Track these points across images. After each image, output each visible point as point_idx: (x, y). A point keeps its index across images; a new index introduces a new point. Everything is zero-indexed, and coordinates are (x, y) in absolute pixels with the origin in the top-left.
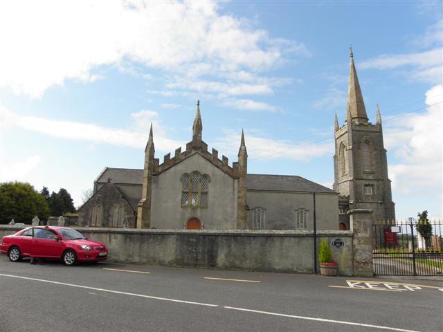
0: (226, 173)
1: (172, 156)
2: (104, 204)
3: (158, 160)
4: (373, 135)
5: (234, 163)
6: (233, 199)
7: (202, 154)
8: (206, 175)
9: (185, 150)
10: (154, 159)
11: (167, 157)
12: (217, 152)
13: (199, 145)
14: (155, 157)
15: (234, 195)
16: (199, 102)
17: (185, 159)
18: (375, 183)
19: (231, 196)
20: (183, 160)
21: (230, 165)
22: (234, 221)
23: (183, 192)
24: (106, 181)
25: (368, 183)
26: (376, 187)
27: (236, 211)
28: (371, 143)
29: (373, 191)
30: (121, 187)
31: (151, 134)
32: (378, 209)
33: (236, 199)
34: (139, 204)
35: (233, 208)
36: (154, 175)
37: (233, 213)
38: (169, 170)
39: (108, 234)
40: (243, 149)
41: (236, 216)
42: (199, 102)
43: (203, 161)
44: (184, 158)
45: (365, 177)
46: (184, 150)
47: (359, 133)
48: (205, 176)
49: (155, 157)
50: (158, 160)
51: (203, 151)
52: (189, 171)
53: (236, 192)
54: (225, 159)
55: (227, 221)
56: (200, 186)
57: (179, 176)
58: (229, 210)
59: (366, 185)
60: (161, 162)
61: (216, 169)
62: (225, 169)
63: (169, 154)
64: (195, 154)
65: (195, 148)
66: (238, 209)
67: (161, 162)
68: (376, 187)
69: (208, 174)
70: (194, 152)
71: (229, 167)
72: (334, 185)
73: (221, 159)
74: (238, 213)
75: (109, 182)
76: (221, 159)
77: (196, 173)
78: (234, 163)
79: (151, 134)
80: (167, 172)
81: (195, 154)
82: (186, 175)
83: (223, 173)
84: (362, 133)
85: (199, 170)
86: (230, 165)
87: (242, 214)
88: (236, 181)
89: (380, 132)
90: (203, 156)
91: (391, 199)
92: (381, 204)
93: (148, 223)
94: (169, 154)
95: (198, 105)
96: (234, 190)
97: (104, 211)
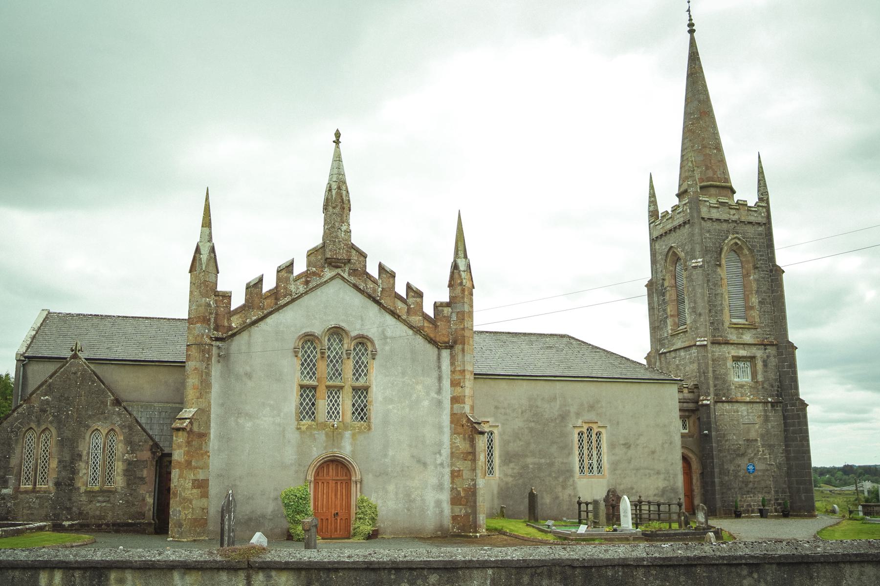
0: (417, 330)
1: (269, 284)
2: (60, 423)
3: (227, 296)
4: (750, 230)
5: (437, 306)
6: (440, 403)
7: (352, 279)
8: (362, 337)
9: (304, 269)
10: (217, 294)
11: (254, 287)
12: (392, 275)
13: (343, 255)
14: (220, 288)
15: (439, 391)
16: (338, 135)
17: (306, 293)
18: (759, 353)
19: (433, 395)
20: (301, 296)
21: (429, 309)
22: (442, 464)
23: (302, 387)
24: (68, 354)
25: (742, 353)
26: (760, 365)
27: (446, 438)
28: (746, 251)
29: (754, 374)
30: (105, 372)
31: (207, 222)
32: (766, 419)
33: (447, 404)
34: (177, 424)
35: (440, 428)
36: (217, 339)
37: (440, 444)
38: (262, 325)
39: (242, 575)
40: (462, 266)
41: (446, 451)
42: (338, 135)
43: (357, 300)
44: (302, 289)
45: (733, 337)
46: (300, 267)
47: (716, 226)
48: (363, 341)
49: (220, 288)
50: (227, 296)
51: (354, 272)
52: (318, 329)
53: (446, 383)
54: (415, 293)
55: (425, 464)
56: (348, 367)
57: (291, 341)
58: (429, 434)
59: (737, 359)
60: (238, 301)
61: (389, 320)
62: (416, 320)
63: (261, 280)
64: (332, 279)
65: (332, 263)
66: (454, 432)
67: (238, 301)
68: (760, 365)
69: (370, 335)
70: (328, 273)
71: (426, 317)
72: (648, 358)
73: (402, 292)
74: (452, 443)
75: (75, 356)
76: (402, 292)
77: (337, 332)
78: (437, 306)
79: (207, 222)
80: (255, 329)
81: (332, 279)
82: (309, 339)
83: (410, 332)
84: (725, 226)
85: (343, 325)
86: (429, 309)
87: (463, 445)
88: (446, 353)
89: (767, 224)
90: (356, 287)
91: (797, 394)
92: (773, 404)
93: (201, 476)
94: (261, 280)
95: (337, 142)
96: (440, 379)
97: (62, 443)
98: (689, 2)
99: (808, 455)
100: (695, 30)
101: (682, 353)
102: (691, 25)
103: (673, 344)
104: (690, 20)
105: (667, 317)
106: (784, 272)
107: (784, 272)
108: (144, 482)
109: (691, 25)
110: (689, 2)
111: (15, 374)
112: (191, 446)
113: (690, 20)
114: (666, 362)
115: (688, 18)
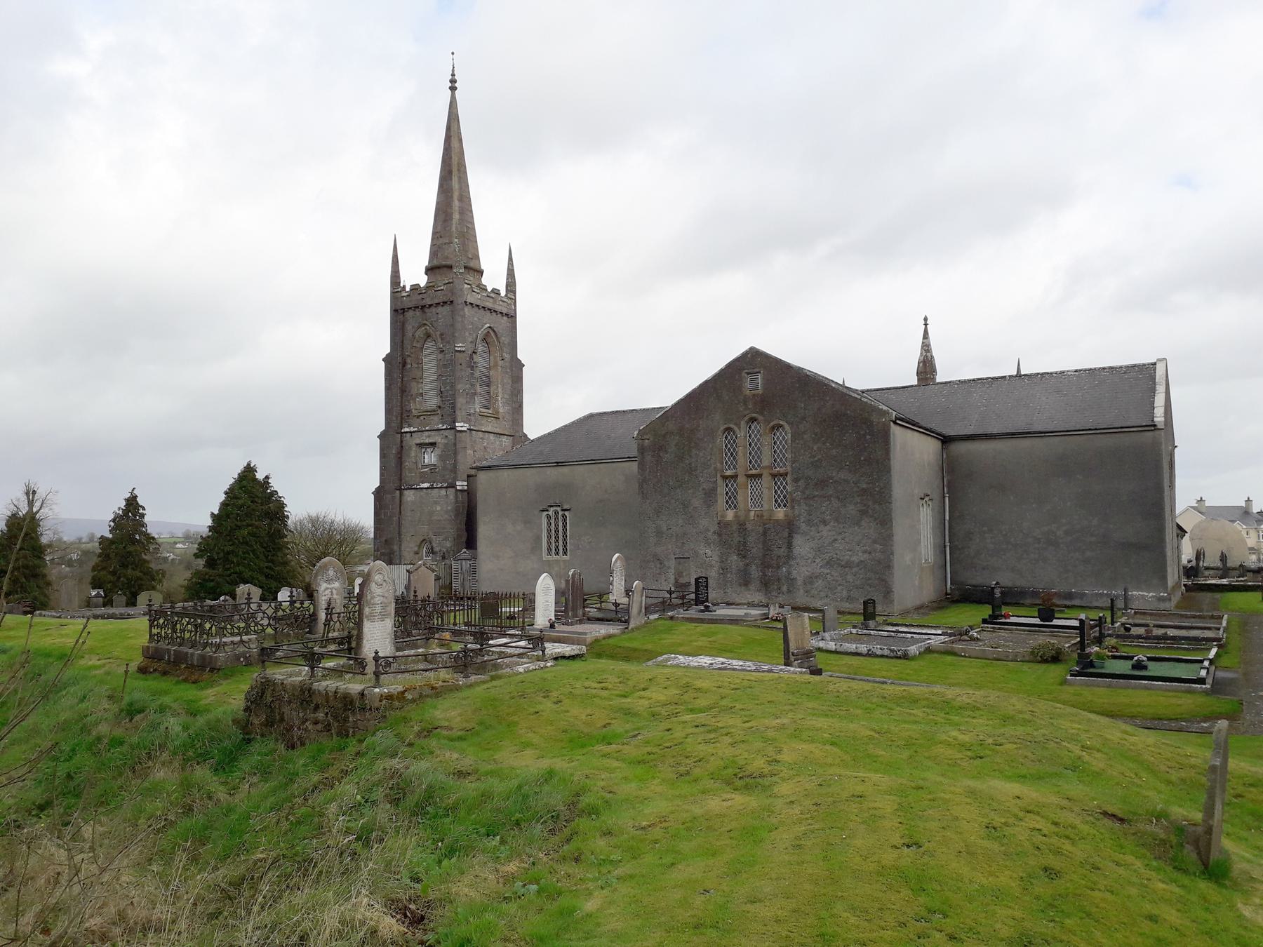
16: (926, 319)
42: (926, 319)
98: (453, 53)
99: (378, 518)
100: (456, 88)
101: (492, 437)
102: (453, 81)
103: (482, 425)
104: (453, 75)
105: (475, 394)
106: (524, 366)
107: (524, 366)
108: (599, 741)
109: (453, 81)
110: (453, 53)
111: (377, 514)
112: (887, 598)
113: (453, 75)
114: (471, 440)
115: (451, 73)
